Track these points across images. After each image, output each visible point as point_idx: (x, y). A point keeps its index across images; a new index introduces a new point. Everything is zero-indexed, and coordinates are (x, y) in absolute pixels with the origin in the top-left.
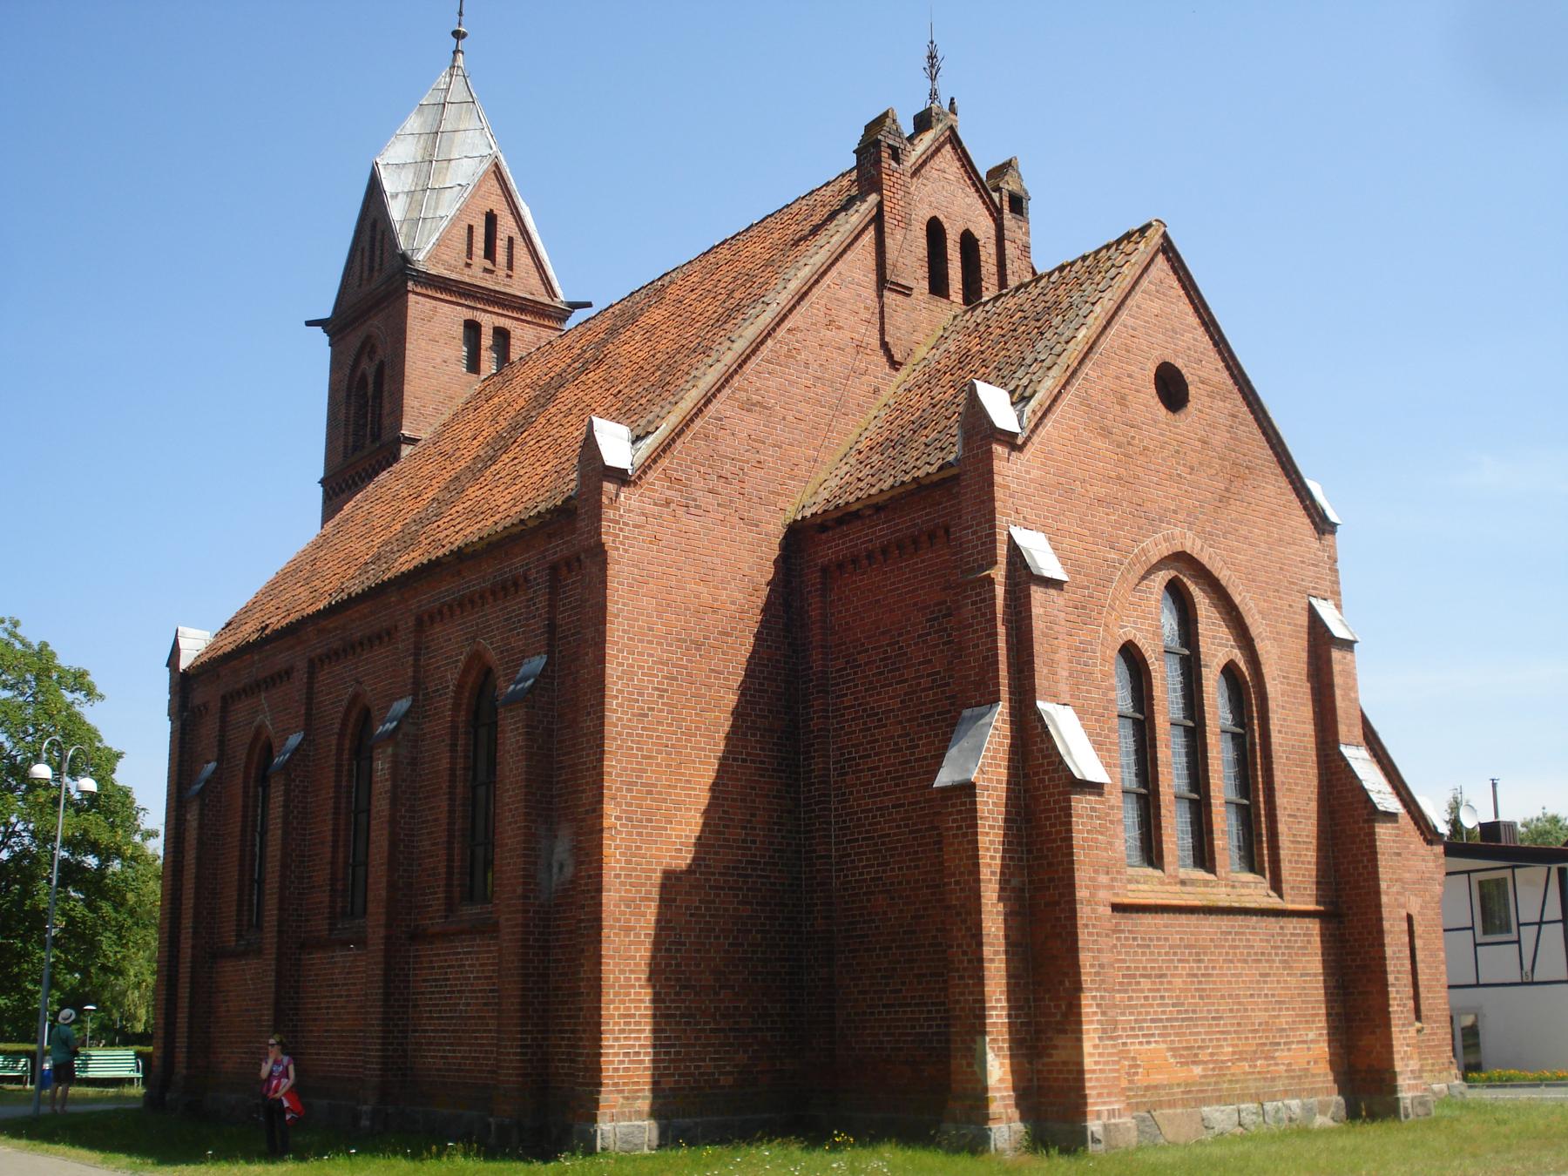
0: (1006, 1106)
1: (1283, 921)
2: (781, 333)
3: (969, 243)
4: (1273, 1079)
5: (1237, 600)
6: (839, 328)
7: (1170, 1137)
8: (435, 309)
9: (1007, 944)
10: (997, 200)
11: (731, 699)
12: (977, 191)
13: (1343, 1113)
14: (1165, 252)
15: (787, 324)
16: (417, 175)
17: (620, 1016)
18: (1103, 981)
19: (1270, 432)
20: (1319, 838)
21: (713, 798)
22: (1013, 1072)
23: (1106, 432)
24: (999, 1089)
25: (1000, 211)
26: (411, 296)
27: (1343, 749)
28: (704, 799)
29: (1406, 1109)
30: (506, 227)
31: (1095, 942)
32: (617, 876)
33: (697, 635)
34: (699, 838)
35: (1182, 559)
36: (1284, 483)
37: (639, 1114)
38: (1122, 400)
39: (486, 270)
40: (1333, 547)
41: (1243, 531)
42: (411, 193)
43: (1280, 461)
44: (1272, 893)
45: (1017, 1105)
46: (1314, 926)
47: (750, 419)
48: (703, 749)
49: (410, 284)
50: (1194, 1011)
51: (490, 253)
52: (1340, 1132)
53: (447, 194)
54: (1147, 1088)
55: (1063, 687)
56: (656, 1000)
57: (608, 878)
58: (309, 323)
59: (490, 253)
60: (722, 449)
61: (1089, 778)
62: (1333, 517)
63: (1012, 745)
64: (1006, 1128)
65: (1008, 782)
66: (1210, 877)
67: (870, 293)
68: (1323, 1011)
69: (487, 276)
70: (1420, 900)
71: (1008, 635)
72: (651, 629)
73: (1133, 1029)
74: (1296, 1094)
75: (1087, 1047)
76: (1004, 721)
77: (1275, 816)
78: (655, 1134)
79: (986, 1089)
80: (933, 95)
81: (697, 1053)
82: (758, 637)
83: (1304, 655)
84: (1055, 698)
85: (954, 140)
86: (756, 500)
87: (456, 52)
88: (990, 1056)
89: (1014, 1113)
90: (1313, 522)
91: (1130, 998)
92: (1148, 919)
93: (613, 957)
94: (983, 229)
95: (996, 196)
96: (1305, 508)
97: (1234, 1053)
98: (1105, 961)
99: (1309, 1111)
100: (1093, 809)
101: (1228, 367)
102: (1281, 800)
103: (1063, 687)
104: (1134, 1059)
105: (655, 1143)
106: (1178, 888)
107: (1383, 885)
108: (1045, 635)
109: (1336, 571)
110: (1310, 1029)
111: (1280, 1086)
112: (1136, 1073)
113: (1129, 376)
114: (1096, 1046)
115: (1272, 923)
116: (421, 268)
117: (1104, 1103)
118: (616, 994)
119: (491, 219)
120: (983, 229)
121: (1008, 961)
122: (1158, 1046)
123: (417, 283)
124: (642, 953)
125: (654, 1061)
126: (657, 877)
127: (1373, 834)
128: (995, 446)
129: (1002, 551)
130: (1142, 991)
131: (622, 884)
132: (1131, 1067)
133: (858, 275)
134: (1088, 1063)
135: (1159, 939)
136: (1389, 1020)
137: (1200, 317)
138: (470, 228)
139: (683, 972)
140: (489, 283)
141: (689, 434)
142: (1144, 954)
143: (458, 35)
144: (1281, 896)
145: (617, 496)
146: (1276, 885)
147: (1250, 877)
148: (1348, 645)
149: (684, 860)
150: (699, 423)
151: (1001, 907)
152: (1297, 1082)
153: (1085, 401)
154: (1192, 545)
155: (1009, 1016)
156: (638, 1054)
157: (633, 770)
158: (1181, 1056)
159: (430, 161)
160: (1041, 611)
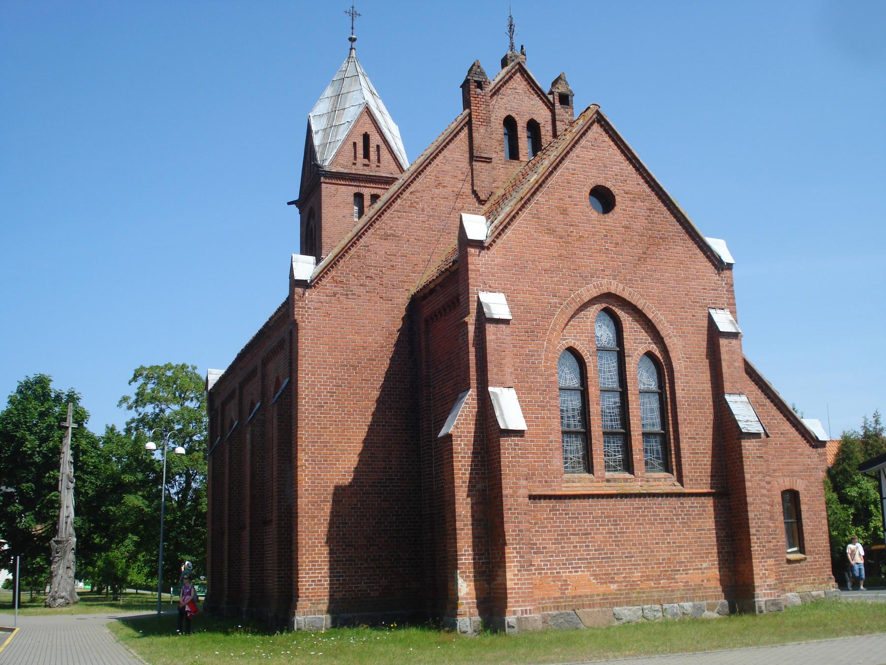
0: (470, 608)
1: (682, 500)
2: (406, 195)
3: (533, 127)
4: (673, 591)
5: (650, 316)
6: (444, 187)
7: (588, 624)
8: (337, 190)
9: (473, 520)
10: (551, 99)
11: (376, 394)
12: (539, 96)
13: (727, 610)
14: (599, 122)
15: (410, 189)
16: (328, 120)
17: (309, 562)
18: (522, 539)
19: (679, 215)
20: (713, 449)
21: (364, 446)
22: (476, 589)
23: (551, 231)
24: (466, 599)
25: (553, 105)
26: (323, 186)
27: (727, 397)
28: (359, 447)
29: (760, 607)
30: (375, 140)
32: (306, 490)
33: (354, 362)
34: (356, 468)
35: (609, 296)
36: (690, 244)
37: (320, 612)
38: (564, 212)
39: (365, 165)
40: (731, 277)
41: (657, 275)
42: (325, 130)
43: (687, 232)
44: (677, 483)
45: (478, 607)
46: (709, 502)
47: (386, 244)
48: (359, 422)
49: (322, 179)
50: (612, 553)
51: (366, 155)
52: (725, 620)
53: (342, 127)
54: (574, 597)
55: (509, 379)
56: (331, 552)
57: (301, 491)
58: (289, 203)
59: (366, 155)
60: (368, 262)
61: (511, 428)
62: (727, 258)
63: (478, 412)
64: (468, 617)
65: (475, 432)
66: (632, 476)
67: (465, 164)
68: (716, 551)
69: (366, 168)
70: (806, 482)
71: (476, 352)
72: (325, 361)
73: (564, 564)
74: (691, 599)
75: (509, 575)
76: (473, 399)
77: (679, 438)
78: (329, 621)
79: (458, 598)
80: (512, 47)
81: (357, 580)
82: (392, 360)
83: (705, 344)
84: (503, 384)
85: (522, 71)
86: (390, 286)
87: (351, 49)
88: (460, 581)
89: (475, 611)
90: (714, 265)
91: (563, 547)
92: (577, 503)
93: (305, 532)
94: (542, 115)
95: (550, 97)
96: (708, 257)
97: (642, 576)
98: (524, 528)
99: (699, 609)
100: (516, 445)
101: (647, 182)
102: (682, 429)
103: (509, 379)
105: (329, 626)
106: (605, 483)
107: (747, 476)
108: (496, 350)
109: (733, 291)
110: (705, 561)
111: (678, 594)
112: (567, 589)
113: (570, 197)
114: (515, 575)
115: (674, 501)
116: (327, 169)
117: (519, 606)
118: (307, 551)
119: (366, 137)
120: (542, 115)
121: (473, 529)
122: (584, 574)
123: (325, 177)
124: (323, 529)
125: (330, 584)
126: (331, 489)
127: (741, 446)
128: (469, 249)
129: (473, 307)
130: (572, 543)
131: (311, 494)
132: (562, 585)
133: (457, 155)
134: (509, 584)
135: (584, 513)
136: (751, 555)
137: (626, 155)
138: (355, 144)
139: (347, 538)
140: (367, 172)
141: (348, 256)
142: (573, 522)
143: (352, 40)
144: (682, 485)
145: (304, 294)
146: (680, 479)
147: (663, 474)
148: (735, 335)
149: (348, 479)
150: (353, 250)
151: (469, 500)
152: (692, 592)
153: (536, 216)
154: (616, 288)
155: (474, 559)
156: (320, 581)
157: (315, 435)
158: (601, 579)
159: (335, 111)
160: (494, 337)
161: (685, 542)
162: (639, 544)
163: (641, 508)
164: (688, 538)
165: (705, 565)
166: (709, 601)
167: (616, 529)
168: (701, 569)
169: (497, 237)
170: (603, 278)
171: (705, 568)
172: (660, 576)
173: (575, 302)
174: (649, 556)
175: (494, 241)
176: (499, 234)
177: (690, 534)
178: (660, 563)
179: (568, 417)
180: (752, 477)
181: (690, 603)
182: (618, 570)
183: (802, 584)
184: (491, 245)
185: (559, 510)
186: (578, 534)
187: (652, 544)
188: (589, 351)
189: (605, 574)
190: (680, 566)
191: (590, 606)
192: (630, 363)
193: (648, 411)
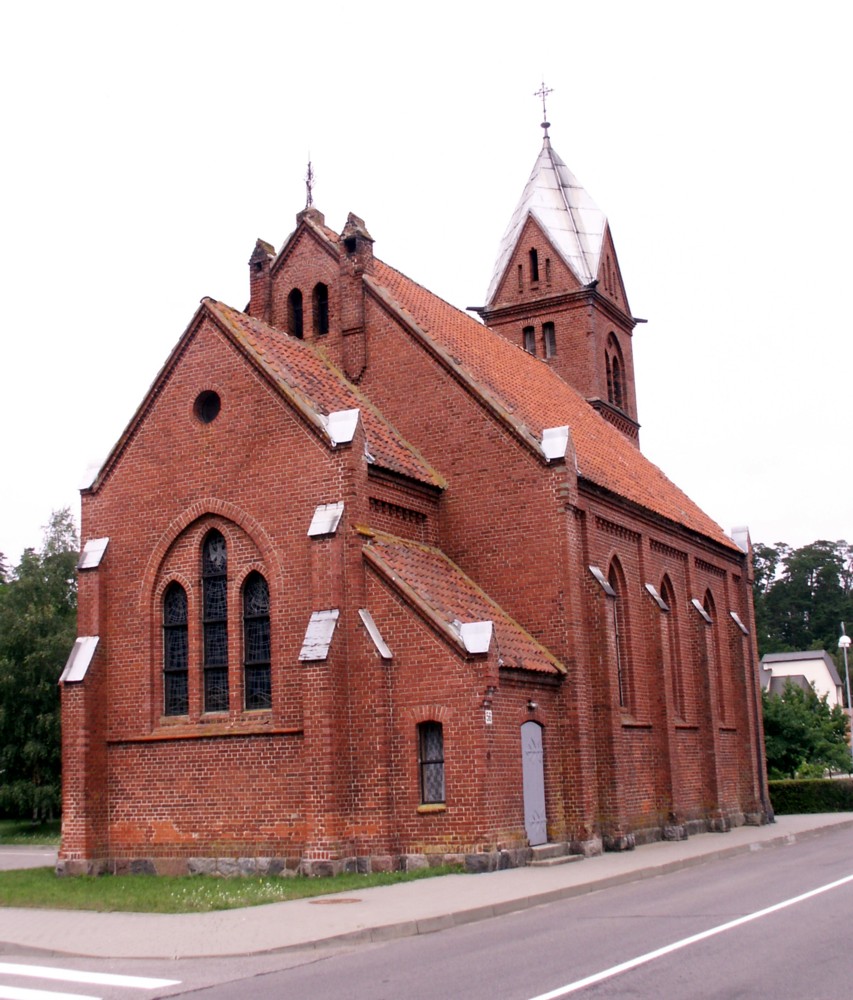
18: (78, 787)
31: (75, 766)
39: (534, 289)
50: (195, 800)
51: (535, 277)
69: (534, 293)
97: (224, 826)
104: (150, 827)
110: (295, 812)
111: (259, 848)
119: (533, 254)
143: (546, 125)
154: (215, 504)
161: (273, 789)
162: (223, 791)
163: (226, 751)
164: (276, 785)
165: (294, 816)
166: (291, 858)
167: (200, 774)
168: (289, 820)
169: (105, 479)
170: (203, 497)
171: (293, 820)
172: (243, 826)
173: (173, 531)
174: (232, 804)
175: (102, 484)
176: (108, 475)
177: (279, 781)
178: (243, 812)
179: (179, 656)
180: (312, 713)
181: (269, 859)
182: (200, 818)
183: (436, 844)
184: (99, 488)
185: (147, 755)
186: (163, 780)
187: (236, 790)
188: (191, 582)
189: (187, 822)
190: (266, 817)
191: (168, 855)
192: (232, 588)
193: (261, 639)
